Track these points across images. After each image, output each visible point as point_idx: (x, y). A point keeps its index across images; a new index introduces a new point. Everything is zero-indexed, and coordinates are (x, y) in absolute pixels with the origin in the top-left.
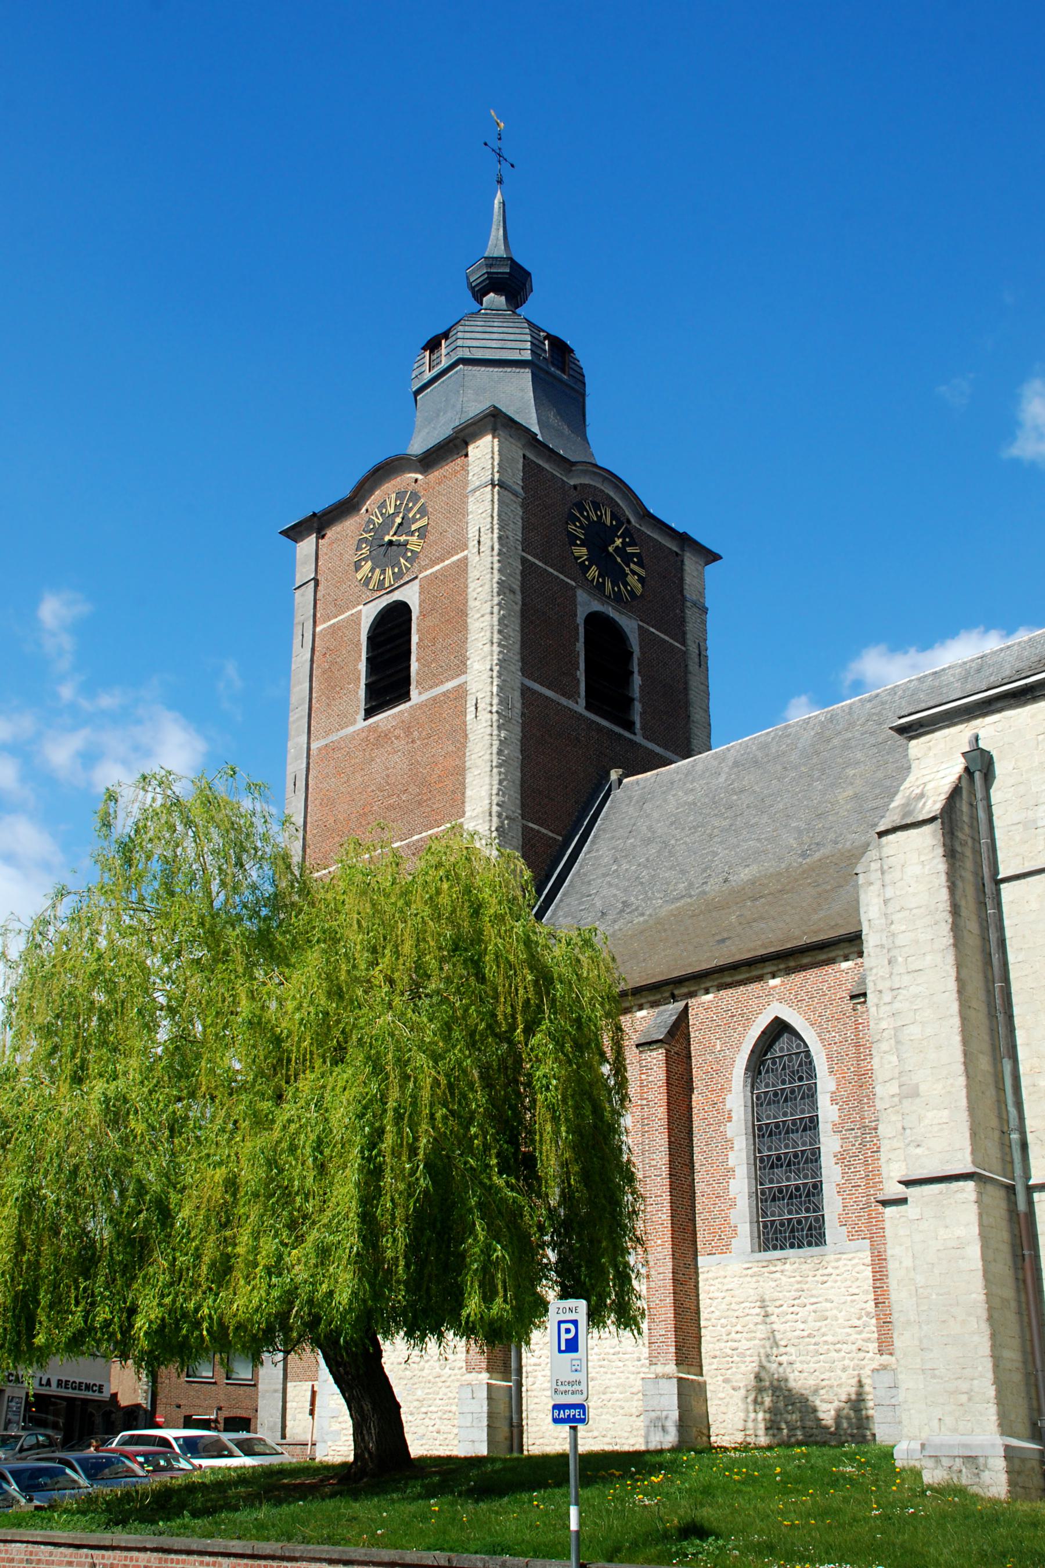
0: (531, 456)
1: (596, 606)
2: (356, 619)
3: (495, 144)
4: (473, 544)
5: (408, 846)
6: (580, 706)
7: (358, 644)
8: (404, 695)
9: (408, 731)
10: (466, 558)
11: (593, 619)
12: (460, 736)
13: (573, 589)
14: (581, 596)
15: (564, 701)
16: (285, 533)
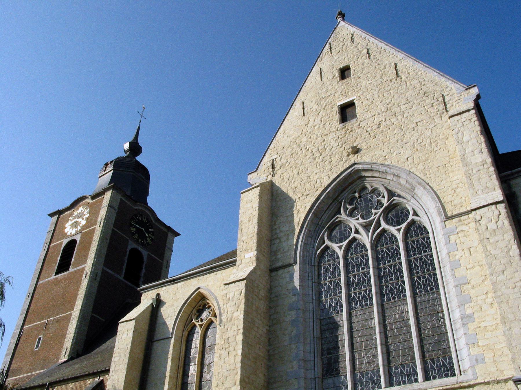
1: (135, 246)
3: (141, 112)
4: (98, 224)
5: (55, 319)
6: (121, 278)
7: (60, 251)
8: (68, 269)
9: (65, 281)
10: (95, 228)
11: (134, 251)
12: (79, 283)
14: (130, 242)
15: (116, 275)
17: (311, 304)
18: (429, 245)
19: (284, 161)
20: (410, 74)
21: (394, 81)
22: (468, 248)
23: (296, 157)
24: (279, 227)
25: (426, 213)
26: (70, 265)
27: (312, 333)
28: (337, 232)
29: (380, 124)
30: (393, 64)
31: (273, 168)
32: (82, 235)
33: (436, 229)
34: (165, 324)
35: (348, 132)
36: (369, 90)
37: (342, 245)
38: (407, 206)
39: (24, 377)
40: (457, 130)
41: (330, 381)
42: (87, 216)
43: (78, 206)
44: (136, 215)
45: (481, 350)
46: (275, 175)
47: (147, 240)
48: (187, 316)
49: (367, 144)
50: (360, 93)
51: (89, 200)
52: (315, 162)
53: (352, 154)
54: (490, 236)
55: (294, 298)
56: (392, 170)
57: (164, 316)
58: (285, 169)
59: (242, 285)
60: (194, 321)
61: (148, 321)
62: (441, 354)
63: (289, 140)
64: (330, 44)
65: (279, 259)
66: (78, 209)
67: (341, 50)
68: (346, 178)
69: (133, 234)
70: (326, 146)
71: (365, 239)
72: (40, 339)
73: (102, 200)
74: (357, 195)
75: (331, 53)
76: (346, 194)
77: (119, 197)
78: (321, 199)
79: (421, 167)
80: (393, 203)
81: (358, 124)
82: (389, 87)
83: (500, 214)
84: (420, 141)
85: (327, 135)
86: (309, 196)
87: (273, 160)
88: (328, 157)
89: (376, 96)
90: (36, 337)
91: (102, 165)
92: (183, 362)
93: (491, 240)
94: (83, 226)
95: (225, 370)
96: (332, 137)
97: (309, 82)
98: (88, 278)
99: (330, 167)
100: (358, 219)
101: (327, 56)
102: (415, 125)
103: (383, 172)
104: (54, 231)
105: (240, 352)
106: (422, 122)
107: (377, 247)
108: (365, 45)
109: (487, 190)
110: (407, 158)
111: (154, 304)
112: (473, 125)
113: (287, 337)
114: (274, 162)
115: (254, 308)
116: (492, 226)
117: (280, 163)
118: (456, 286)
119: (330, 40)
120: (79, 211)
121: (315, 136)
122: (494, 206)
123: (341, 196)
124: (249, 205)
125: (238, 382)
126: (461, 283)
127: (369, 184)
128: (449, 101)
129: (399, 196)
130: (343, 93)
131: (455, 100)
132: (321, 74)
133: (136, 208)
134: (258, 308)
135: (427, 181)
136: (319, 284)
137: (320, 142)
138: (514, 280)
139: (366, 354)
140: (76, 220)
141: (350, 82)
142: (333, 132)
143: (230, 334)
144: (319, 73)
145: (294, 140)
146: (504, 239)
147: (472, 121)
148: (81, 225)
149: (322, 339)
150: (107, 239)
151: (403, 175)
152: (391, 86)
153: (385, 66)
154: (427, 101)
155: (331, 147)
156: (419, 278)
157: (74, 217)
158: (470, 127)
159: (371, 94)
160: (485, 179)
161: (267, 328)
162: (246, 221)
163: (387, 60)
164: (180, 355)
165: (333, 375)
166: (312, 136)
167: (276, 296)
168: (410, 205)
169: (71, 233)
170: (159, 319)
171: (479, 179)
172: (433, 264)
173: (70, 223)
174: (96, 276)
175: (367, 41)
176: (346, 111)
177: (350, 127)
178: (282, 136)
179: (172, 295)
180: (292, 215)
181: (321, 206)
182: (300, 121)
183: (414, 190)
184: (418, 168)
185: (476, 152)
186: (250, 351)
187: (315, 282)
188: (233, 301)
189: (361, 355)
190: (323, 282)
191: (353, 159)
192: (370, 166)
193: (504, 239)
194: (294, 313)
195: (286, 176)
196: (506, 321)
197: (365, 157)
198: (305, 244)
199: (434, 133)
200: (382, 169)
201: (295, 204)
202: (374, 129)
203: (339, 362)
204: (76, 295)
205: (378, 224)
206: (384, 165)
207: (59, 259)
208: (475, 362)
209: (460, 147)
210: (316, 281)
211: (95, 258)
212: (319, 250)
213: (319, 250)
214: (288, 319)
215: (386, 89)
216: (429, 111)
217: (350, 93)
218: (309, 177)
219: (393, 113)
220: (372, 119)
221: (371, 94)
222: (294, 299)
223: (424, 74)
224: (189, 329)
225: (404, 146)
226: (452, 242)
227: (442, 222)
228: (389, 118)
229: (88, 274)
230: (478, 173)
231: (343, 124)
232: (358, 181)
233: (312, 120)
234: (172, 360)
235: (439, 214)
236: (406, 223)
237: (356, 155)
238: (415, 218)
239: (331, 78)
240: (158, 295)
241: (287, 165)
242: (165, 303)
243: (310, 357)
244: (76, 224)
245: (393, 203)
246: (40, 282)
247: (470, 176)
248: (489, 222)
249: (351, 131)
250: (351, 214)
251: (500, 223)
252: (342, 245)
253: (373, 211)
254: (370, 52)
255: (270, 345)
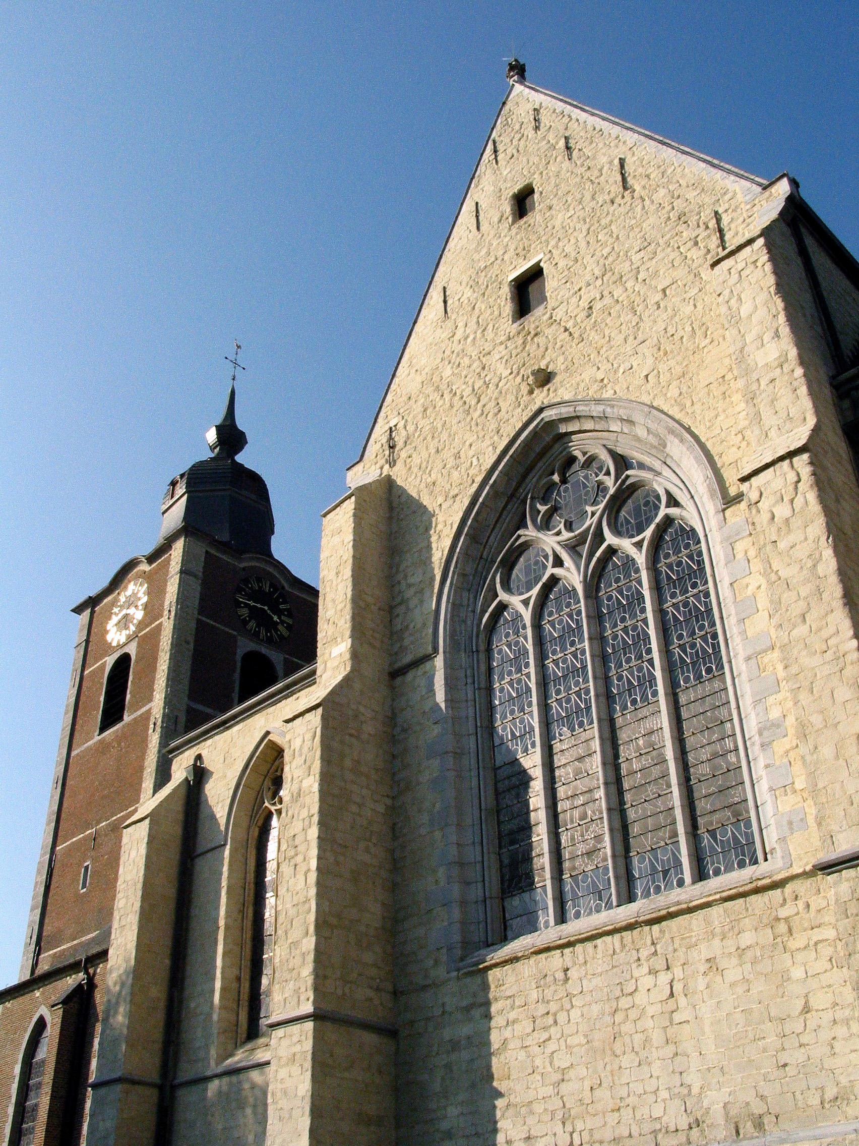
0: (213, 552)
1: (252, 646)
2: (104, 665)
4: (166, 613)
7: (102, 684)
8: (121, 718)
10: (161, 624)
12: (145, 741)
13: (235, 637)
16: (73, 611)
17: (473, 738)
18: (702, 570)
19: (411, 428)
20: (652, 177)
21: (618, 200)
22: (769, 562)
23: (433, 415)
24: (406, 577)
25: (692, 497)
26: (124, 709)
27: (476, 801)
28: (520, 570)
29: (590, 308)
30: (616, 162)
31: (392, 447)
32: (138, 643)
33: (711, 531)
34: (213, 817)
35: (529, 338)
36: (570, 231)
37: (530, 597)
38: (656, 486)
39: (69, 948)
40: (726, 293)
41: (516, 901)
42: (145, 599)
43: (126, 581)
44: (246, 581)
45: (800, 798)
46: (395, 462)
47: (277, 630)
48: (253, 794)
49: (566, 359)
50: (553, 243)
51: (144, 567)
52: (469, 419)
53: (538, 387)
54: (779, 536)
55: (437, 730)
56: (615, 410)
57: (212, 801)
58: (413, 445)
59: (315, 719)
60: (266, 804)
61: (181, 817)
62: (729, 819)
63: (419, 379)
64: (494, 142)
65: (406, 648)
66: (126, 588)
67: (515, 152)
68: (527, 444)
69: (245, 622)
70: (487, 379)
71: (573, 576)
72: (87, 868)
73: (168, 561)
74: (556, 478)
75: (497, 162)
76: (532, 480)
77: (201, 549)
78: (481, 500)
79: (673, 392)
80: (628, 483)
81: (548, 315)
82: (609, 218)
83: (799, 481)
84: (671, 330)
85: (489, 353)
86: (458, 498)
87: (391, 428)
88: (493, 403)
89: (583, 244)
90: (80, 865)
91: (166, 487)
92: (252, 892)
93: (782, 545)
94: (140, 622)
95: (289, 906)
96: (498, 357)
97: (456, 240)
98: (158, 730)
99: (496, 425)
100: (559, 533)
101: (489, 171)
102: (660, 295)
103: (600, 417)
104: (87, 641)
105: (314, 864)
106: (673, 287)
107: (598, 589)
108: (562, 131)
109: (788, 426)
110: (647, 376)
111: (191, 778)
112: (761, 274)
113: (425, 818)
114: (394, 434)
115: (348, 763)
116: (782, 511)
117: (404, 433)
118: (748, 659)
119: (494, 135)
120: (129, 592)
121: (466, 361)
122: (787, 462)
123: (524, 486)
124: (337, 539)
125: (312, 928)
126: (758, 649)
127: (578, 448)
128: (729, 224)
129: (641, 466)
130: (519, 250)
131: (741, 219)
132: (477, 217)
133: (242, 565)
134: (358, 762)
135: (687, 422)
136: (490, 690)
137: (478, 371)
138: (825, 634)
139: (582, 836)
140: (124, 612)
141: (532, 222)
142: (501, 343)
143: (297, 827)
144: (474, 214)
145: (429, 378)
146: (806, 539)
147: (759, 264)
148: (135, 621)
149: (498, 812)
150: (188, 643)
151: (638, 417)
152: (613, 215)
153: (601, 170)
154: (684, 234)
155: (496, 380)
156: (682, 647)
157: (121, 606)
158: (753, 281)
159: (573, 241)
160: (785, 399)
161: (389, 802)
162: (331, 575)
163: (604, 155)
164: (245, 878)
165: (521, 888)
166: (462, 361)
167: (404, 730)
168: (660, 484)
169: (118, 642)
170: (202, 806)
171: (773, 402)
172: (709, 611)
173: (115, 619)
174: (176, 723)
175: (566, 120)
176: (526, 291)
178: (406, 372)
179: (222, 755)
180: (429, 547)
181: (480, 518)
182: (439, 331)
183: (665, 446)
184: (669, 395)
185: (767, 338)
186: (341, 859)
187: (479, 689)
188: (301, 755)
189: (573, 839)
190: (497, 685)
192: (572, 409)
193: (806, 539)
194: (436, 763)
195: (416, 460)
196: (807, 732)
197: (563, 390)
198: (455, 607)
199: (700, 306)
200: (596, 410)
201: (434, 519)
202: (579, 321)
203: (532, 859)
204: (141, 769)
205: (599, 537)
206: (598, 401)
207: (102, 699)
208: (786, 828)
209: (735, 332)
210: (483, 685)
212: (487, 615)
213: (487, 615)
214: (425, 777)
215: (603, 222)
216: (688, 257)
217: (533, 246)
218: (457, 456)
219: (617, 276)
220: (574, 300)
221: (573, 241)
222: (436, 731)
223: (679, 170)
224: (260, 823)
225: (639, 349)
226: (740, 556)
227: (717, 512)
228: (609, 289)
229: (159, 723)
230: (771, 386)
231: (518, 323)
232: (556, 446)
233: (461, 325)
234: (228, 892)
235: (712, 496)
236: (652, 527)
237: (546, 388)
238: (673, 511)
239: (496, 219)
240: (199, 757)
241: (416, 435)
242: (212, 773)
243: (473, 854)
244: (125, 621)
245: (628, 483)
247: (753, 399)
248: (777, 502)
249: (536, 335)
250: (546, 525)
251: (799, 502)
252: (530, 597)
253: (589, 509)
254: (572, 143)
255: (395, 838)
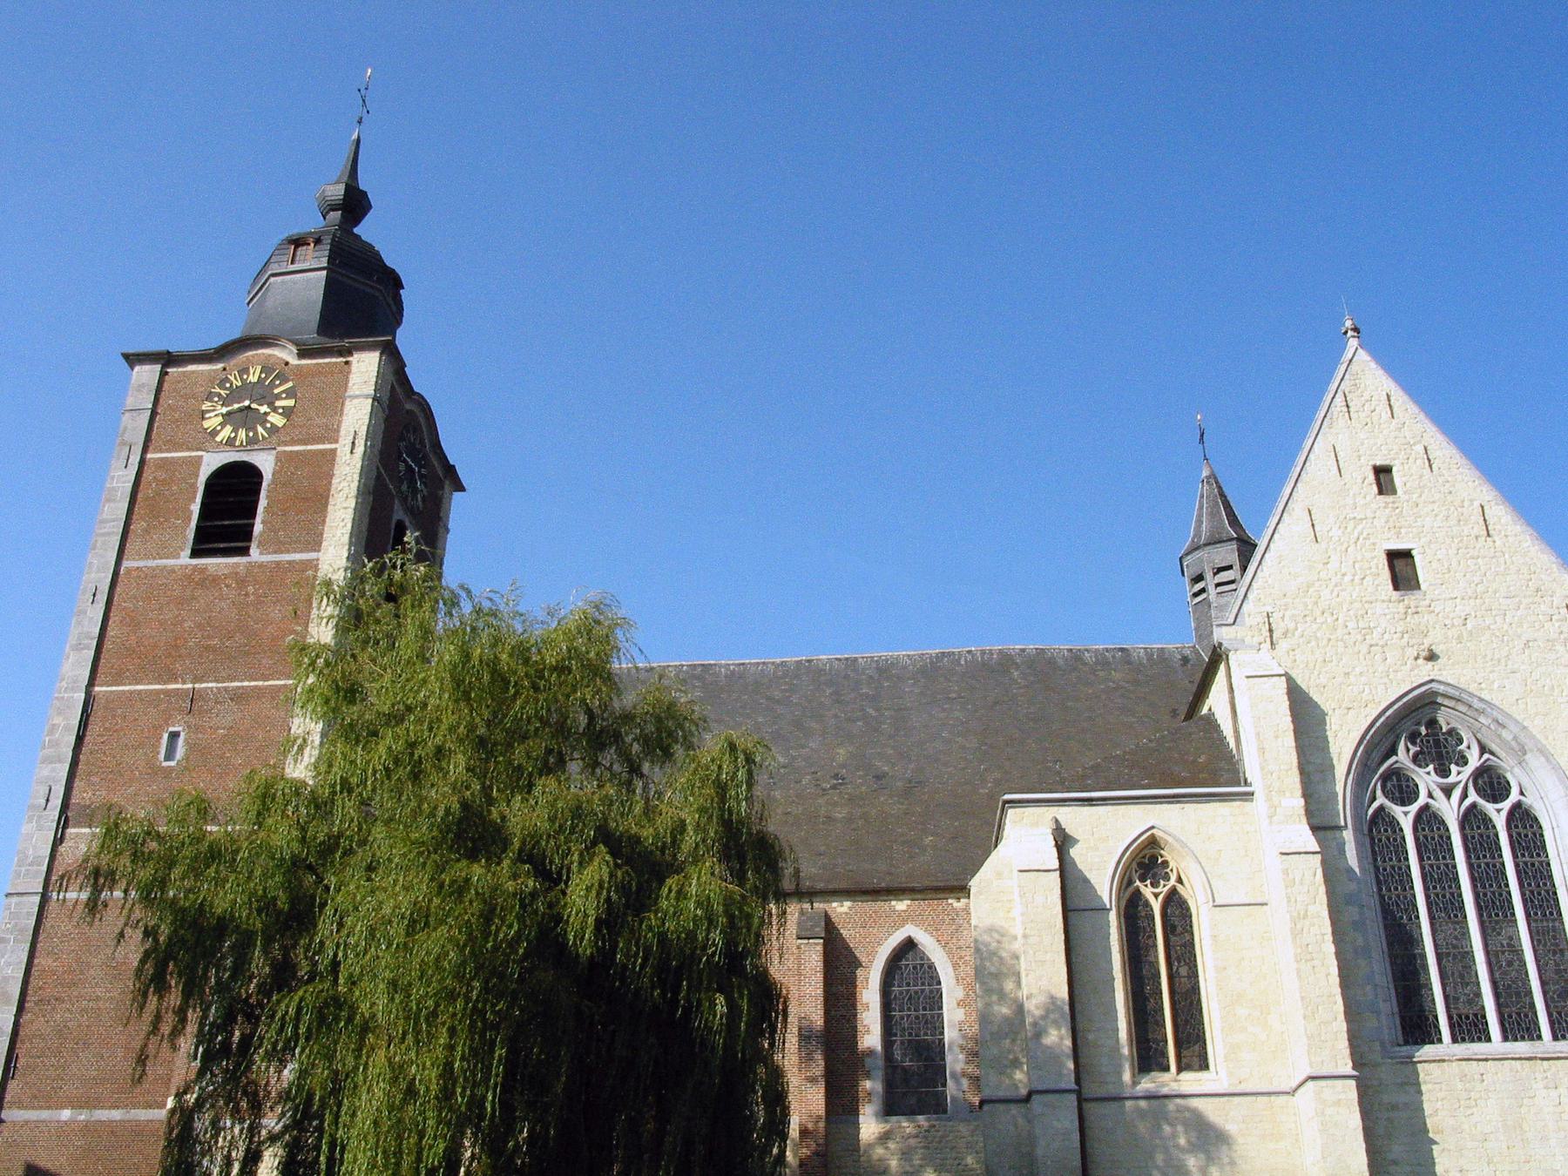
7: (194, 487)
30: (1477, 504)
76: (1408, 726)
177: (1412, 604)
191: (1425, 671)
197: (1448, 673)
200: (1476, 704)
206: (1481, 700)
207: (196, 508)
211: (351, 544)
246: (126, 564)
